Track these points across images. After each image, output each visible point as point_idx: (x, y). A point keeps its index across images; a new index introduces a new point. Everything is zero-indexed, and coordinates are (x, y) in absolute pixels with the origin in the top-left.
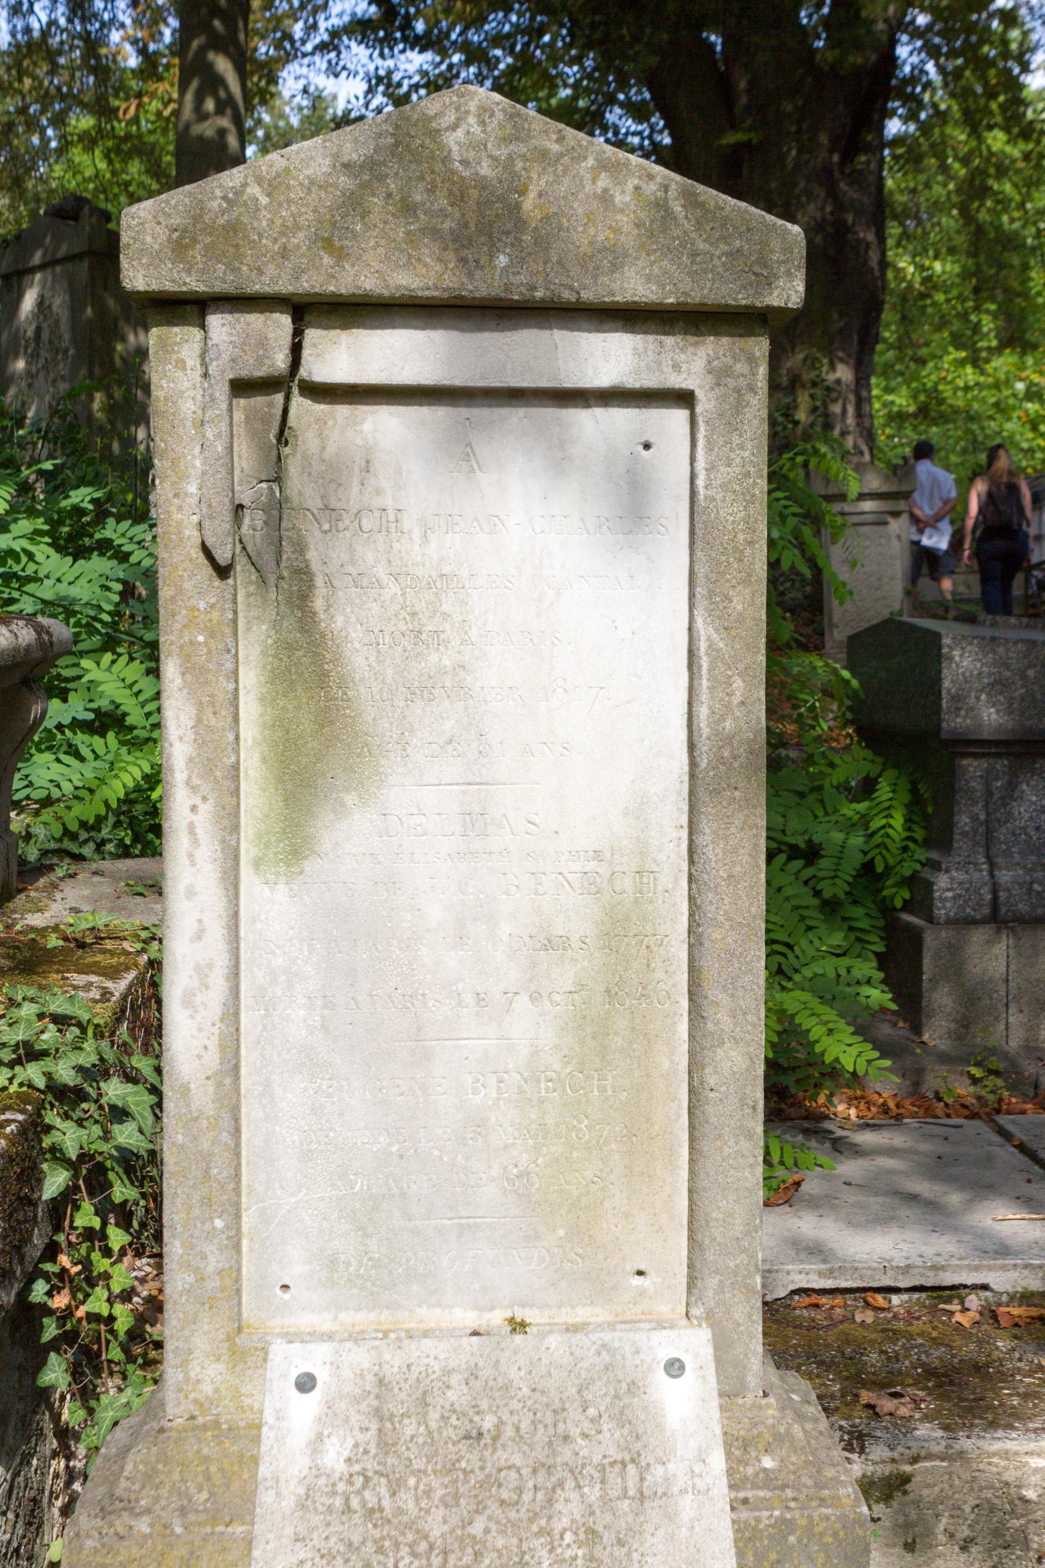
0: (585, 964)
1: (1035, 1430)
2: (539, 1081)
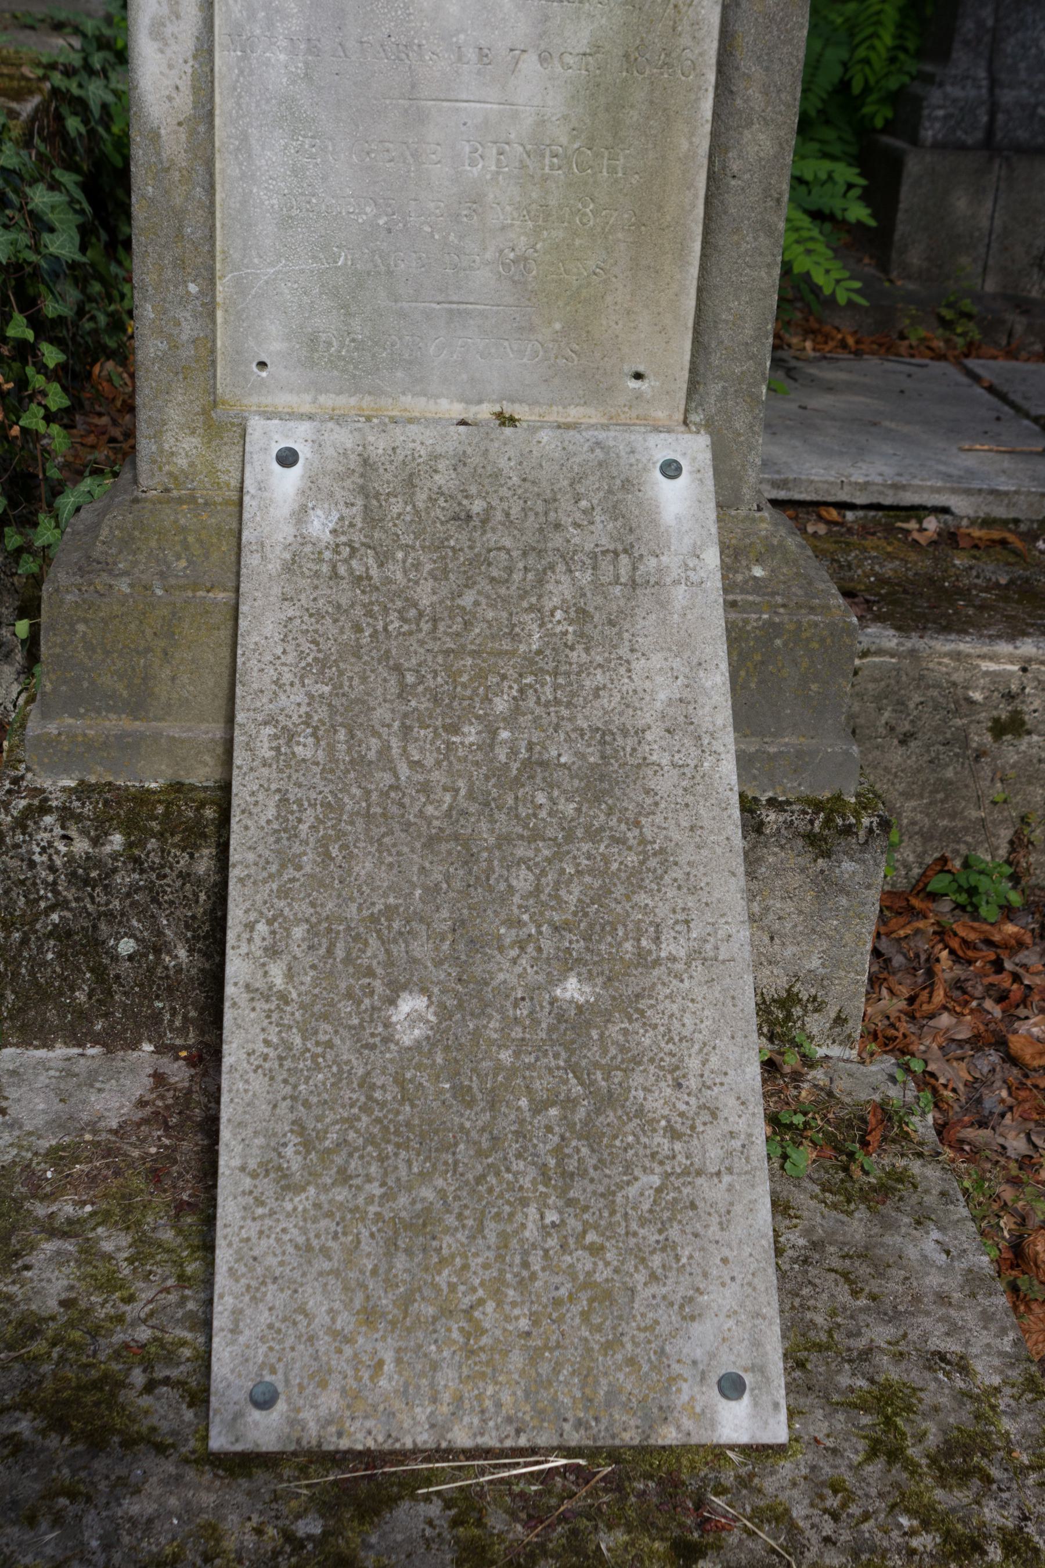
0: (603, 21)
1: (990, 637)
2: (543, 156)
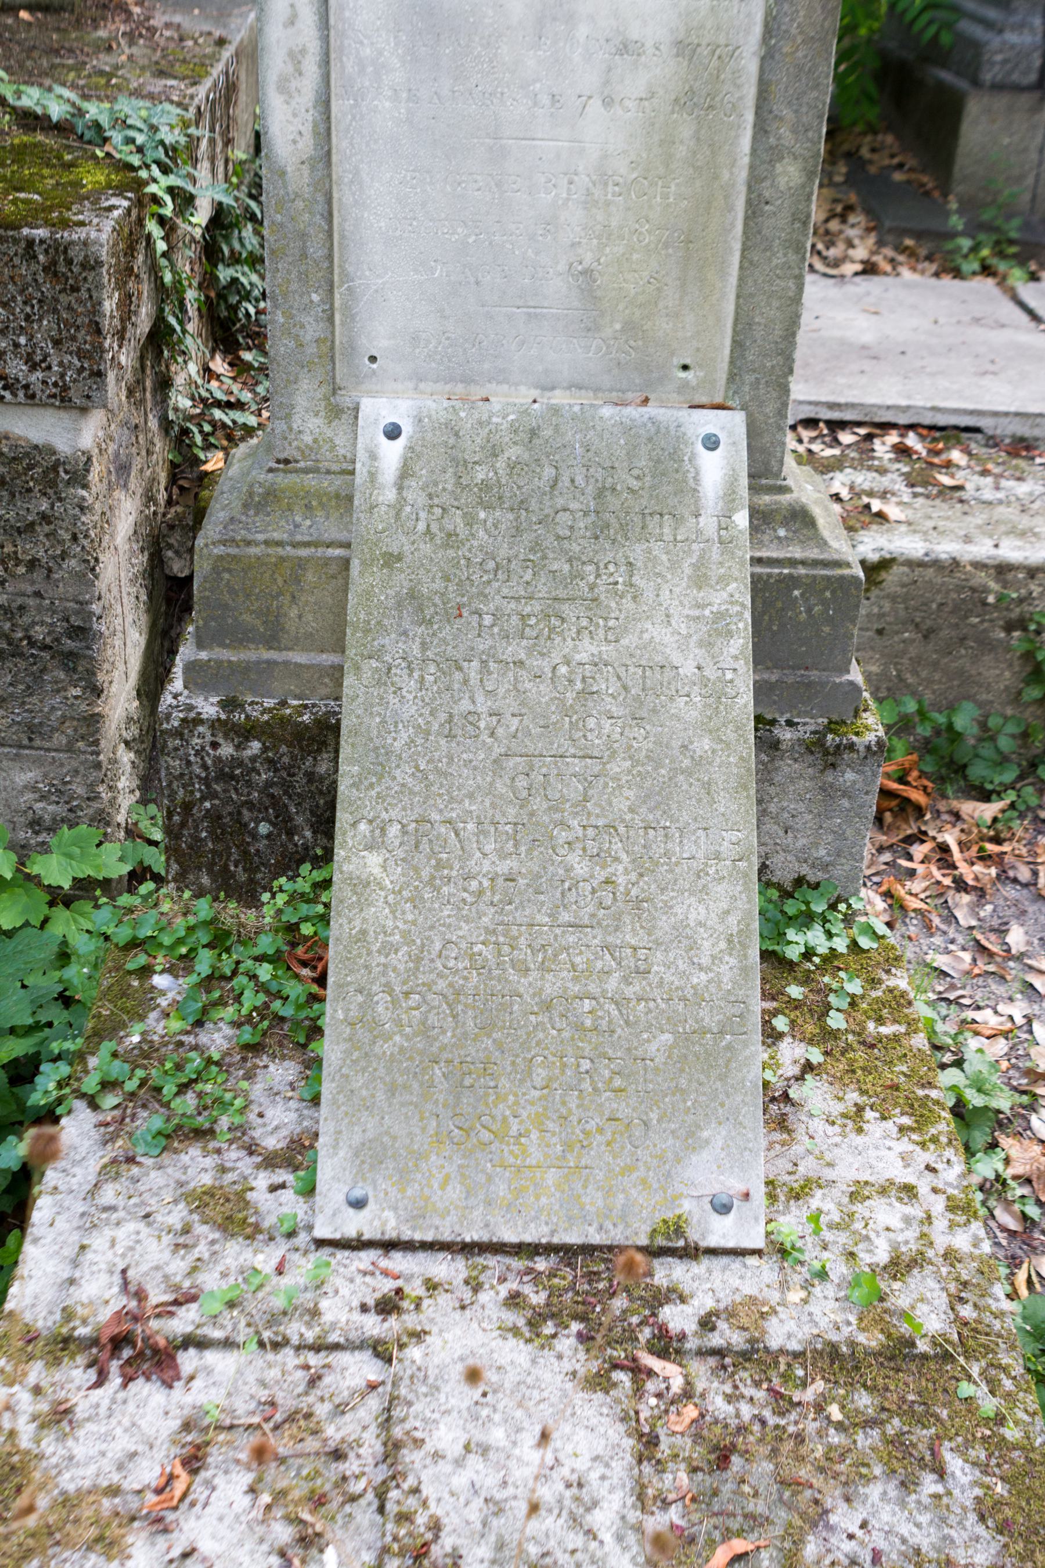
2: (606, 184)
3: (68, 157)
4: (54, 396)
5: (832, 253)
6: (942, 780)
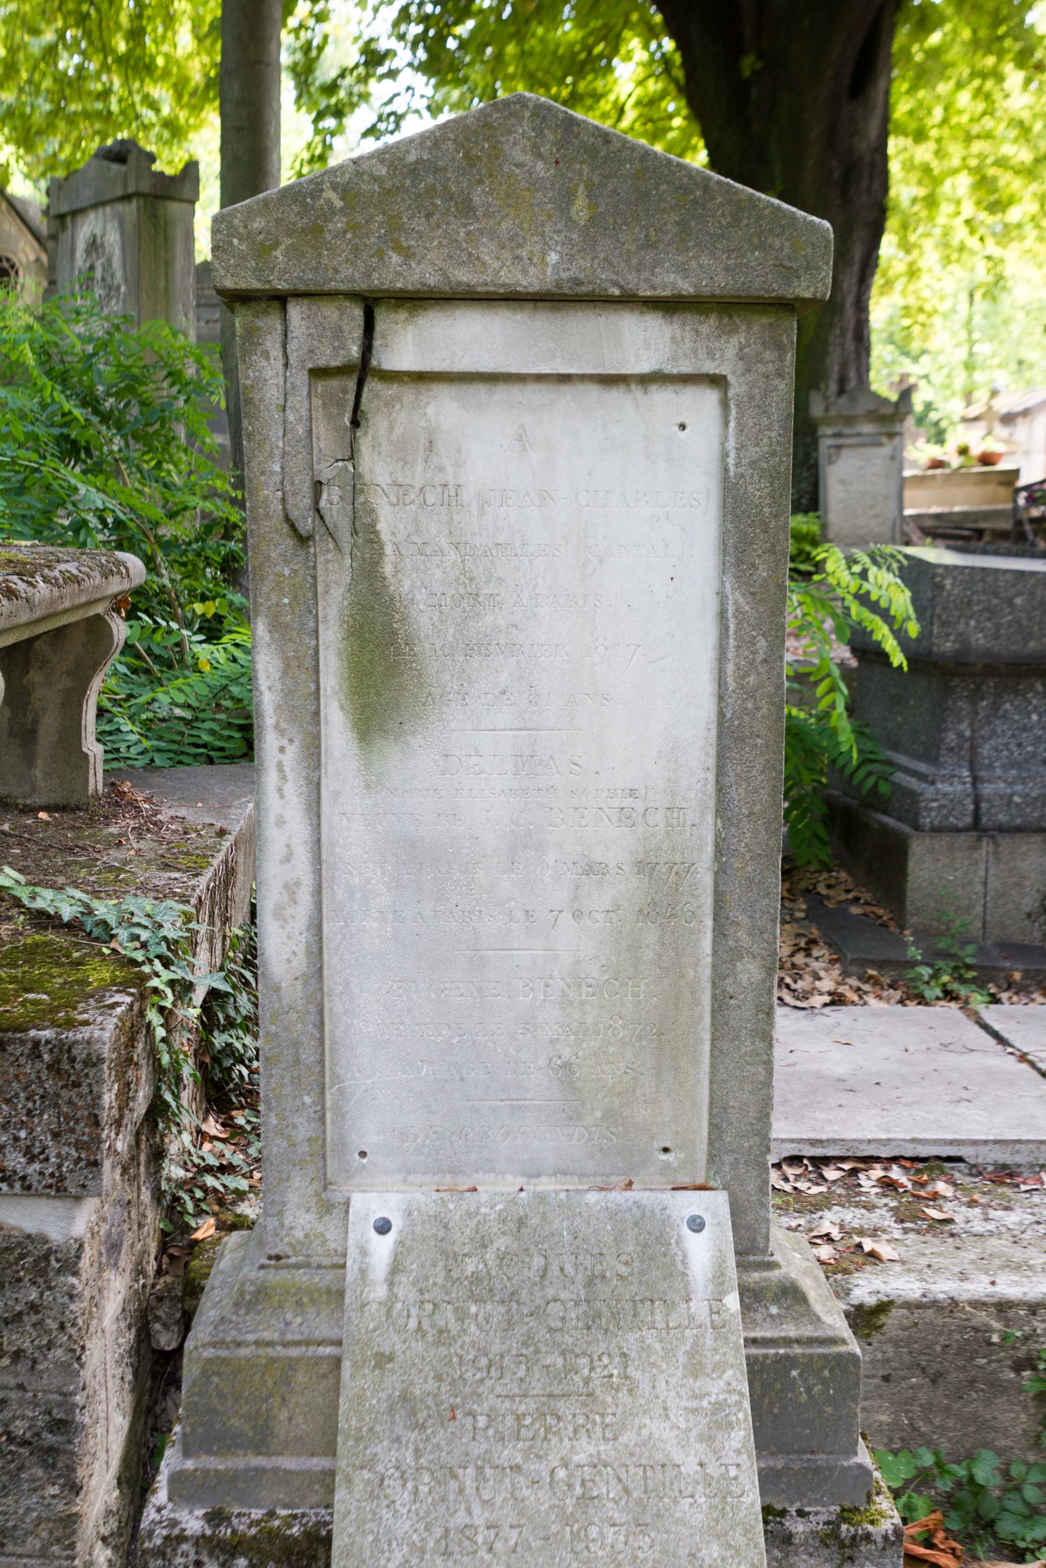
2: (580, 986)
3: (76, 955)
4: (50, 1186)
5: (800, 985)
6: (970, 1538)
